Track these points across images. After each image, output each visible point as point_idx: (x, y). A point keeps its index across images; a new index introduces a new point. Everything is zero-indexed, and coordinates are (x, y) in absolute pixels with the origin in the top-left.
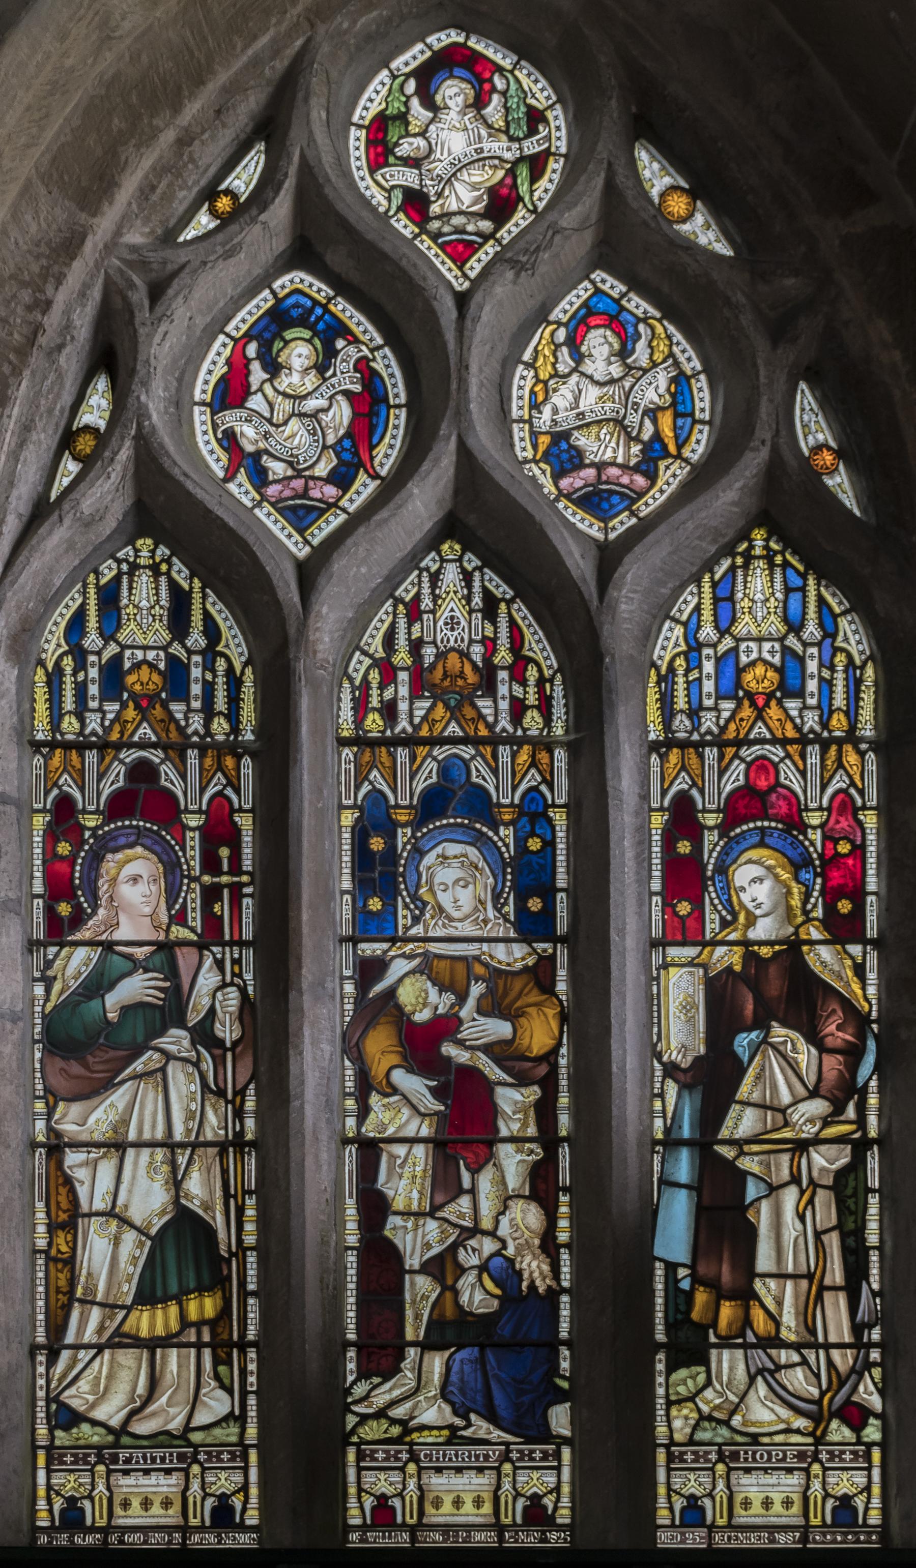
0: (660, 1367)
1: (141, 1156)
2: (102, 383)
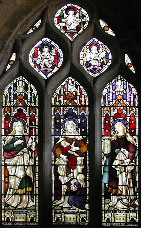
0: (103, 199)
1: (19, 167)
2: (14, 54)
